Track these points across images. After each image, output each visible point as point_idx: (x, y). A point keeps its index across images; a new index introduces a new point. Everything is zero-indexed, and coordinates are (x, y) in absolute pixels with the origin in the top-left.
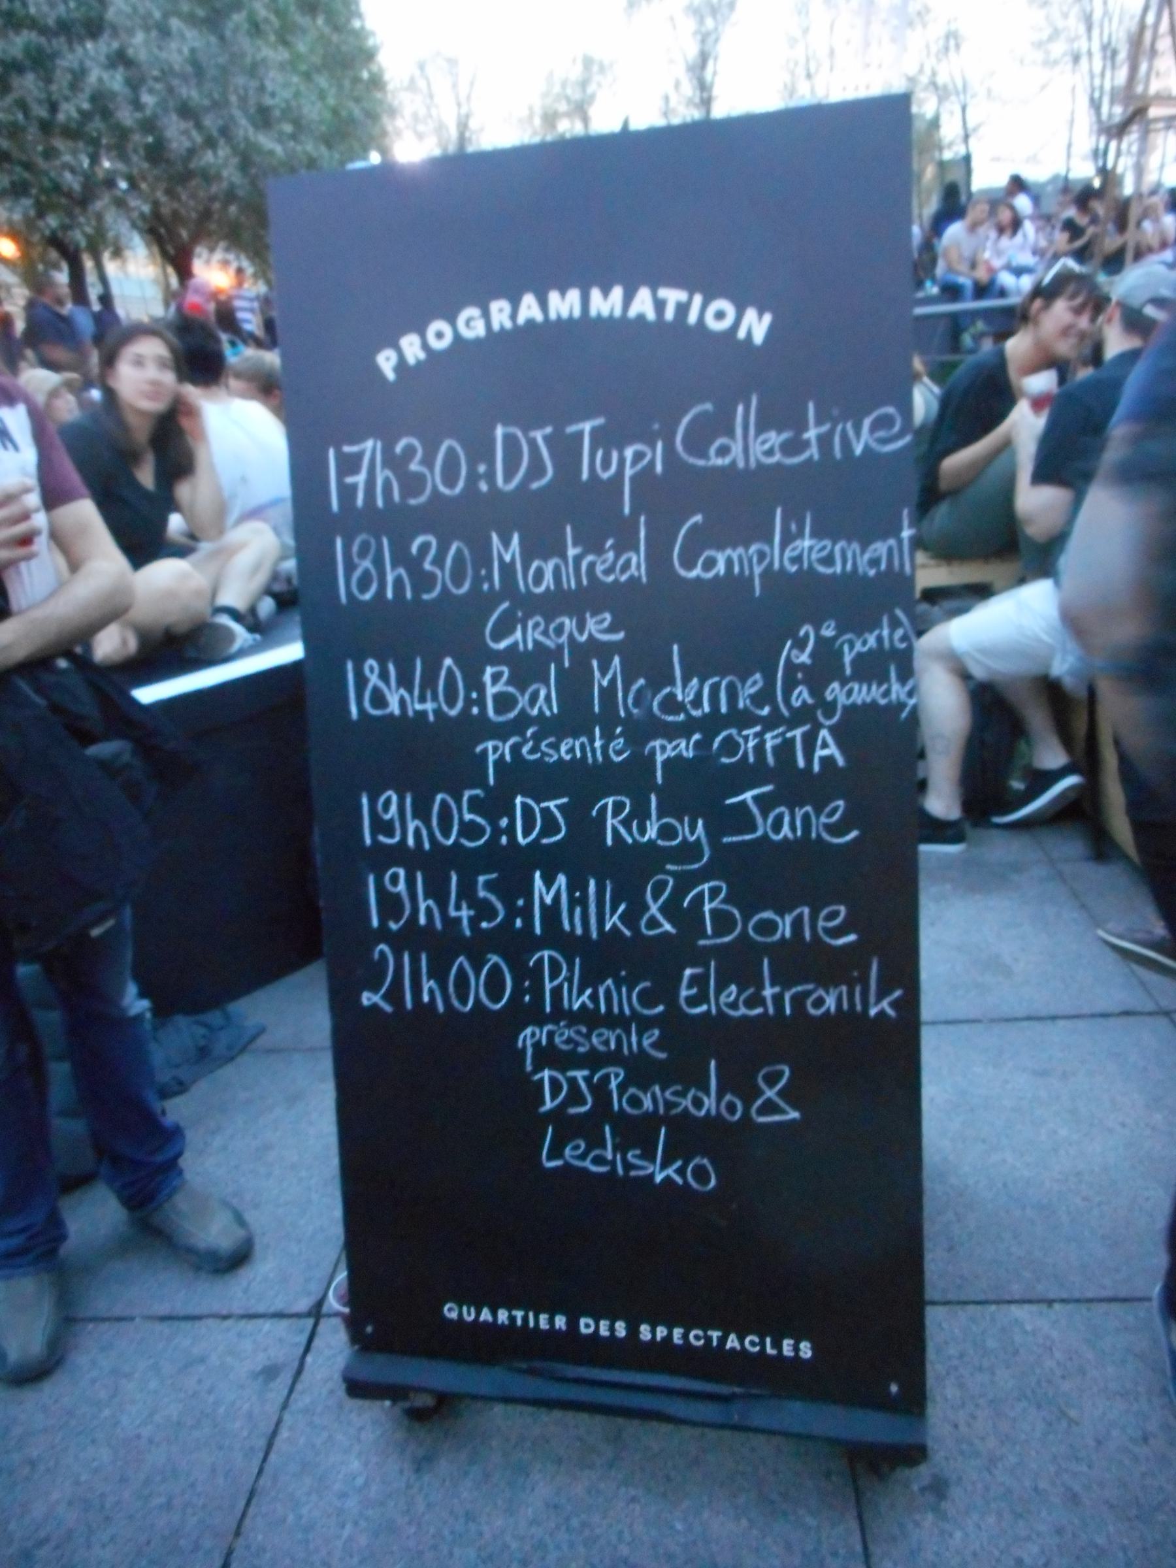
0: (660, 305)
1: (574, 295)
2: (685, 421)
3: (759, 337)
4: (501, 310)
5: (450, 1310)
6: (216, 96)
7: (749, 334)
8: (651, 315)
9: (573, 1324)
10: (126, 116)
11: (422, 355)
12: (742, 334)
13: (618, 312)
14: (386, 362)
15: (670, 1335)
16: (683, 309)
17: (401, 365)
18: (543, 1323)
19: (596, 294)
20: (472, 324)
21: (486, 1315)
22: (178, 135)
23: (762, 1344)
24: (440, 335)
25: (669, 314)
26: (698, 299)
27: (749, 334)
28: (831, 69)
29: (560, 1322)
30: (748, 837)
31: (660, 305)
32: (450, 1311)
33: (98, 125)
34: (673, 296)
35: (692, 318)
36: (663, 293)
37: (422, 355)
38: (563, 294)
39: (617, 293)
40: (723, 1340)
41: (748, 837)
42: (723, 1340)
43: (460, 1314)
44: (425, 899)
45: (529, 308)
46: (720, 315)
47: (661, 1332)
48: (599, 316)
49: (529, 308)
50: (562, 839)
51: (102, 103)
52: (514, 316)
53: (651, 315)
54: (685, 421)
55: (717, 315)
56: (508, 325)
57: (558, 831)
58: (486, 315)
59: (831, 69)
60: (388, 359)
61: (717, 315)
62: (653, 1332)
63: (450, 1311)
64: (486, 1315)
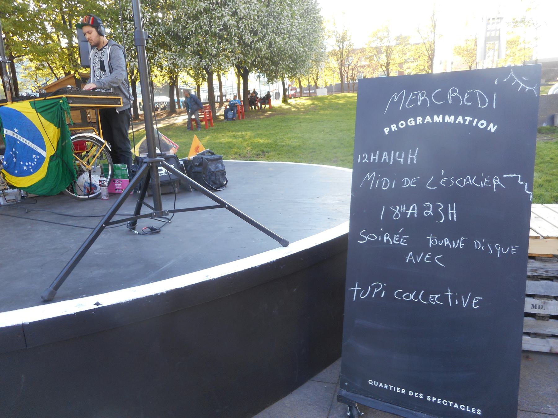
1: (452, 117)
2: (435, 92)
5: (371, 382)
8: (462, 122)
9: (407, 392)
10: (233, 31)
12: (489, 129)
14: (386, 130)
15: (437, 400)
16: (471, 122)
18: (398, 390)
19: (447, 117)
21: (381, 385)
22: (248, 37)
23: (466, 408)
24: (402, 124)
29: (403, 391)
31: (465, 121)
32: (371, 382)
33: (224, 35)
39: (441, 117)
40: (453, 405)
42: (453, 405)
43: (373, 383)
45: (428, 119)
46: (482, 124)
47: (434, 399)
49: (428, 119)
51: (226, 27)
54: (435, 92)
62: (431, 399)
63: (371, 382)
64: (381, 385)
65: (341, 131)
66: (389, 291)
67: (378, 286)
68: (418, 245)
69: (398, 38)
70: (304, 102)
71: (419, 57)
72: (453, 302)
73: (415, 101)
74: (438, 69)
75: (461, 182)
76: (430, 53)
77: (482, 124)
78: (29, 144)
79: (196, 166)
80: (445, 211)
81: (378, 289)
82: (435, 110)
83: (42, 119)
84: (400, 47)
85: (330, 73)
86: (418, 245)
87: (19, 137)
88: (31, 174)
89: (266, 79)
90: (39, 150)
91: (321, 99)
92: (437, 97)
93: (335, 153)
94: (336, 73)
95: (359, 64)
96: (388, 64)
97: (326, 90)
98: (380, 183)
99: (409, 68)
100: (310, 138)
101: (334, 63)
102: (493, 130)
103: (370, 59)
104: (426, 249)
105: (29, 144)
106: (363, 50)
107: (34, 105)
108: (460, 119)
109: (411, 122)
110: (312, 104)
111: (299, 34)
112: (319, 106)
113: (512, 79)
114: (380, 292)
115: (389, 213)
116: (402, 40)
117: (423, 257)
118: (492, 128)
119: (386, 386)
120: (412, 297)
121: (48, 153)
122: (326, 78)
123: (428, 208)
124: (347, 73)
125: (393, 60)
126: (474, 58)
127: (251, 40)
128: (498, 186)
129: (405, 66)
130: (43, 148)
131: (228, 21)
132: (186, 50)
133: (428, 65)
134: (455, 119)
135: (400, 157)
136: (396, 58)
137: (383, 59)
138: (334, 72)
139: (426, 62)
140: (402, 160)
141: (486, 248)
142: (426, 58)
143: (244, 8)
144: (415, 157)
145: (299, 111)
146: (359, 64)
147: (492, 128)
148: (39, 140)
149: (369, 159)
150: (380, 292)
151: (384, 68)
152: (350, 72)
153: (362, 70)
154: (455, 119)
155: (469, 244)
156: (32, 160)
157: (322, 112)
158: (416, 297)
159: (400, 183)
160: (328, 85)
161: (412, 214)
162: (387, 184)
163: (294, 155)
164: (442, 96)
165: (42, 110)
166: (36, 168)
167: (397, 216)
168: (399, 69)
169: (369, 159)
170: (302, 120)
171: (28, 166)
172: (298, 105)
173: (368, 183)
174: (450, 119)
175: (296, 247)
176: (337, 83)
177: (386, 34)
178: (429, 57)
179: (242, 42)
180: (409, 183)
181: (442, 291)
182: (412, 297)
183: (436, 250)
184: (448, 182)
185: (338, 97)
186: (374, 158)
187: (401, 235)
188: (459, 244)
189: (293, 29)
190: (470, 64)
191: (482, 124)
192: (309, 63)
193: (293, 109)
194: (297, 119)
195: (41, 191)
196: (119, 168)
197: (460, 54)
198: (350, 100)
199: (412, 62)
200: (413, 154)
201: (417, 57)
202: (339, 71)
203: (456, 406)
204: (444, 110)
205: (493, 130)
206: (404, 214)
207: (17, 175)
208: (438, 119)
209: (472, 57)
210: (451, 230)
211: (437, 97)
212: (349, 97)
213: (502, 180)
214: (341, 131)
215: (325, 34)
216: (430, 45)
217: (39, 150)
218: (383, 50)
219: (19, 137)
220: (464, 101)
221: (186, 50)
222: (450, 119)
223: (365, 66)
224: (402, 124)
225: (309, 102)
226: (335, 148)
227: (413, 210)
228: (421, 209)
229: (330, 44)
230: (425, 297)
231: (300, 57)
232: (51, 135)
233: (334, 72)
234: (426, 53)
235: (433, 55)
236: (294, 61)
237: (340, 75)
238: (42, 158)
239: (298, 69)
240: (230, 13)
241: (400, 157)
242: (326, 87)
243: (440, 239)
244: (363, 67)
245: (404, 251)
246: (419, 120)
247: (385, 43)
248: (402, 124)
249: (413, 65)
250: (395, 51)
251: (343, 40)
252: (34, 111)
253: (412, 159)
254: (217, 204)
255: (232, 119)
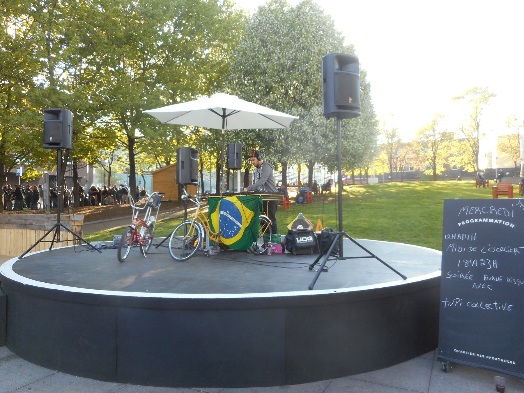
1: (493, 220)
14: (459, 224)
16: (502, 222)
22: (321, 140)
29: (474, 354)
32: (455, 350)
45: (480, 220)
47: (490, 357)
63: (455, 350)
64: (461, 352)
65: (402, 217)
66: (464, 302)
67: (458, 300)
68: (479, 280)
69: (444, 135)
70: (357, 189)
71: (464, 152)
72: (498, 307)
73: (474, 211)
74: (483, 165)
75: (499, 250)
76: (474, 149)
77: (507, 224)
78: (233, 220)
79: (325, 238)
80: (492, 263)
81: (458, 302)
82: (483, 216)
83: (244, 206)
84: (445, 143)
85: (380, 164)
86: (479, 280)
87: (229, 216)
88: (232, 237)
89: (327, 170)
90: (239, 224)
91: (373, 187)
92: (484, 210)
93: (401, 235)
94: (385, 164)
95: (407, 156)
96: (435, 157)
97: (377, 179)
98: (457, 249)
99: (454, 161)
100: (377, 222)
101: (384, 156)
102: (512, 227)
103: (417, 152)
104: (482, 282)
105: (233, 220)
106: (409, 145)
107: (239, 199)
108: (496, 221)
109: (472, 221)
110: (367, 192)
111: (360, 137)
112: (374, 194)
113: (520, 205)
114: (459, 303)
115: (462, 264)
116: (446, 137)
117: (481, 285)
118: (512, 226)
119: (464, 352)
120: (476, 305)
121: (243, 227)
122: (376, 168)
123: (483, 262)
124: (396, 164)
125: (439, 154)
126: (518, 154)
127: (323, 142)
128: (517, 253)
129: (451, 159)
130: (241, 222)
131: (306, 129)
132: (271, 150)
133: (473, 159)
134: (494, 221)
135: (467, 237)
136: (442, 152)
137: (430, 153)
138: (383, 163)
139: (471, 157)
140: (468, 238)
141: (513, 281)
142: (471, 153)
143: (319, 119)
144: (475, 237)
145: (356, 199)
146: (407, 156)
147: (512, 226)
148: (239, 217)
149: (451, 237)
150: (459, 303)
151: (431, 161)
152: (399, 164)
153: (410, 162)
154: (494, 221)
155: (504, 279)
156: (234, 230)
157: (378, 200)
158: (479, 305)
159: (467, 250)
160: (378, 174)
161: (475, 264)
162: (461, 250)
163: (367, 234)
164: (487, 210)
165: (243, 201)
166: (235, 234)
167: (467, 265)
168: (444, 162)
169: (451, 237)
170: (364, 207)
171: (231, 233)
172: (354, 192)
173: (451, 249)
174: (491, 221)
175: (409, 281)
176: (386, 172)
177: (431, 133)
178: (474, 152)
179: (316, 145)
180: (472, 249)
181: (492, 302)
182: (476, 305)
183: (488, 282)
184: (492, 250)
185: (389, 186)
186: (454, 237)
187: (469, 274)
188: (499, 279)
189: (356, 134)
190: (514, 159)
191: (507, 224)
192: (366, 158)
193: (351, 196)
194: (359, 205)
195: (237, 248)
196: (276, 237)
197: (504, 151)
198: (401, 189)
199: (457, 156)
200: (474, 236)
201: (462, 152)
202: (388, 162)
203: (502, 360)
204: (489, 216)
205: (512, 227)
206: (471, 264)
207: (226, 238)
208: (485, 220)
209: (516, 153)
210: (494, 273)
211: (484, 210)
212: (399, 186)
213: (519, 250)
214: (402, 217)
215: (378, 133)
216: (474, 142)
217: (239, 224)
218: (430, 145)
219: (229, 216)
220: (498, 212)
221: (271, 150)
222: (491, 221)
223: (412, 159)
224: (467, 222)
225: (363, 190)
226: (399, 231)
227: (474, 262)
228: (479, 262)
229: (381, 140)
230: (483, 306)
231: (359, 154)
232: (247, 216)
233: (383, 163)
234: (471, 149)
235: (478, 151)
236: (354, 157)
237: (389, 166)
238: (239, 228)
239: (357, 162)
240: (308, 123)
241: (467, 237)
242: (376, 176)
243: (490, 277)
244: (410, 159)
245: (472, 283)
246: (476, 220)
247: (432, 139)
248: (467, 222)
249: (458, 159)
250: (440, 147)
251: (393, 136)
252: (239, 202)
253: (473, 238)
254: (370, 256)
255: (302, 203)
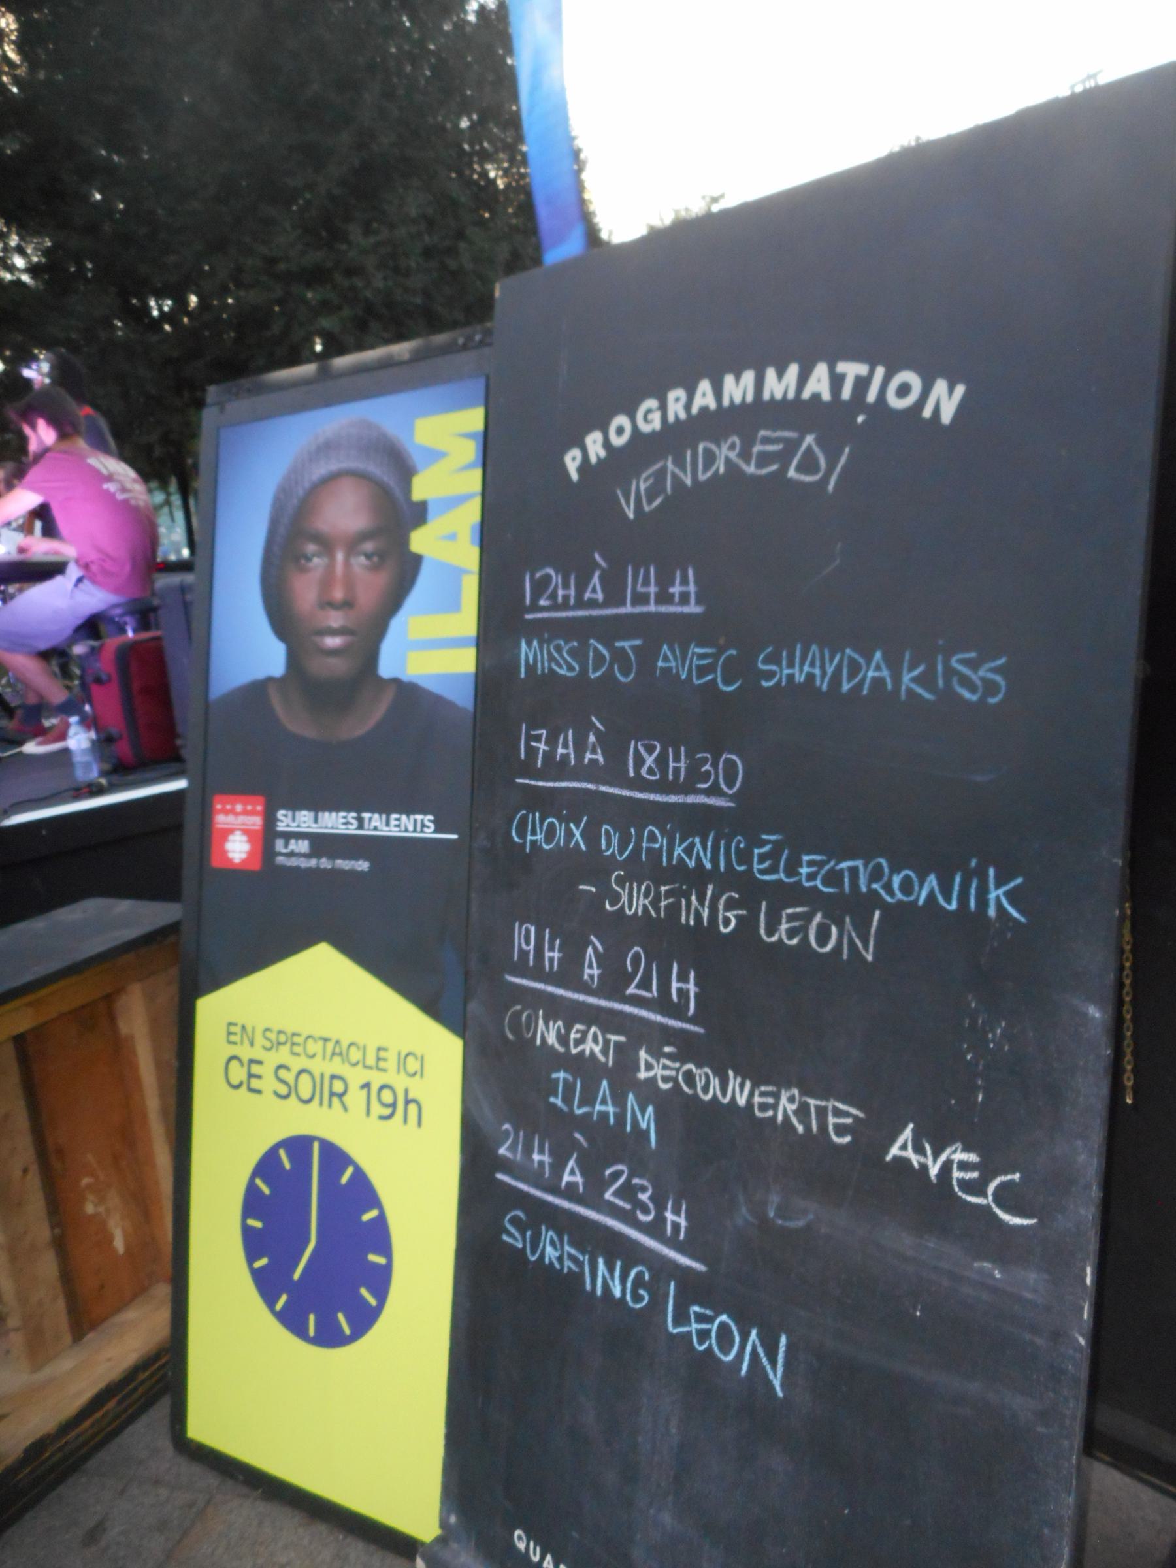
0: (837, 381)
3: (946, 417)
4: (677, 400)
6: (282, 266)
7: (951, 390)
8: (826, 396)
11: (603, 454)
13: (791, 395)
16: (862, 384)
17: (584, 466)
20: (650, 417)
25: (846, 393)
26: (880, 371)
27: (951, 390)
28: (419, 1124)
30: (670, 1319)
34: (851, 370)
35: (872, 396)
36: (841, 367)
37: (603, 454)
38: (738, 378)
39: (793, 370)
41: (670, 1319)
44: (529, 951)
45: (705, 396)
48: (380, 814)
49: (705, 396)
50: (772, 687)
52: (688, 407)
53: (826, 396)
55: (901, 389)
56: (683, 415)
57: (726, 759)
58: (663, 408)
59: (419, 1124)
60: (574, 459)
61: (901, 389)
